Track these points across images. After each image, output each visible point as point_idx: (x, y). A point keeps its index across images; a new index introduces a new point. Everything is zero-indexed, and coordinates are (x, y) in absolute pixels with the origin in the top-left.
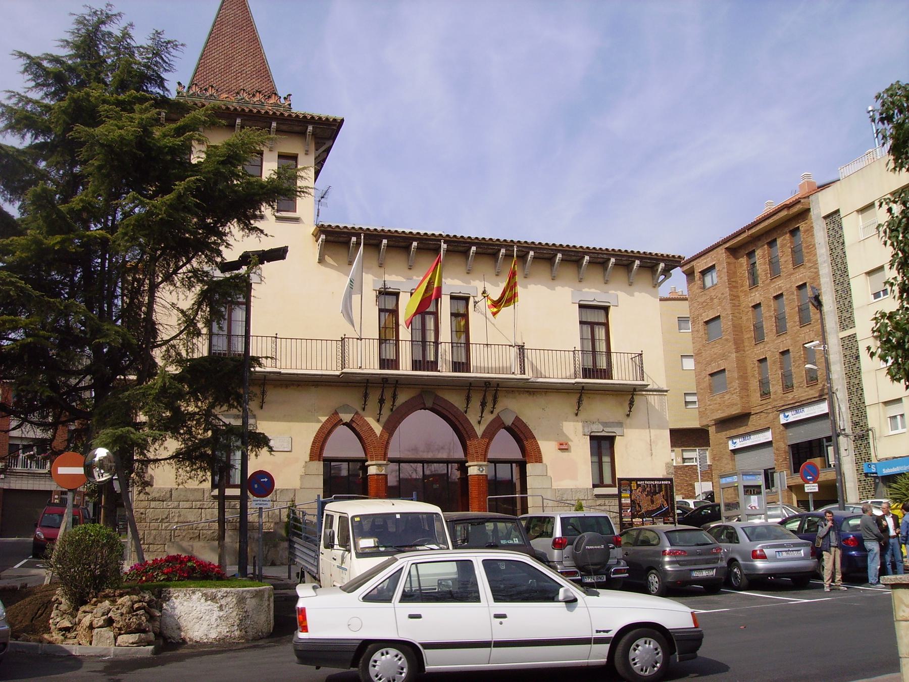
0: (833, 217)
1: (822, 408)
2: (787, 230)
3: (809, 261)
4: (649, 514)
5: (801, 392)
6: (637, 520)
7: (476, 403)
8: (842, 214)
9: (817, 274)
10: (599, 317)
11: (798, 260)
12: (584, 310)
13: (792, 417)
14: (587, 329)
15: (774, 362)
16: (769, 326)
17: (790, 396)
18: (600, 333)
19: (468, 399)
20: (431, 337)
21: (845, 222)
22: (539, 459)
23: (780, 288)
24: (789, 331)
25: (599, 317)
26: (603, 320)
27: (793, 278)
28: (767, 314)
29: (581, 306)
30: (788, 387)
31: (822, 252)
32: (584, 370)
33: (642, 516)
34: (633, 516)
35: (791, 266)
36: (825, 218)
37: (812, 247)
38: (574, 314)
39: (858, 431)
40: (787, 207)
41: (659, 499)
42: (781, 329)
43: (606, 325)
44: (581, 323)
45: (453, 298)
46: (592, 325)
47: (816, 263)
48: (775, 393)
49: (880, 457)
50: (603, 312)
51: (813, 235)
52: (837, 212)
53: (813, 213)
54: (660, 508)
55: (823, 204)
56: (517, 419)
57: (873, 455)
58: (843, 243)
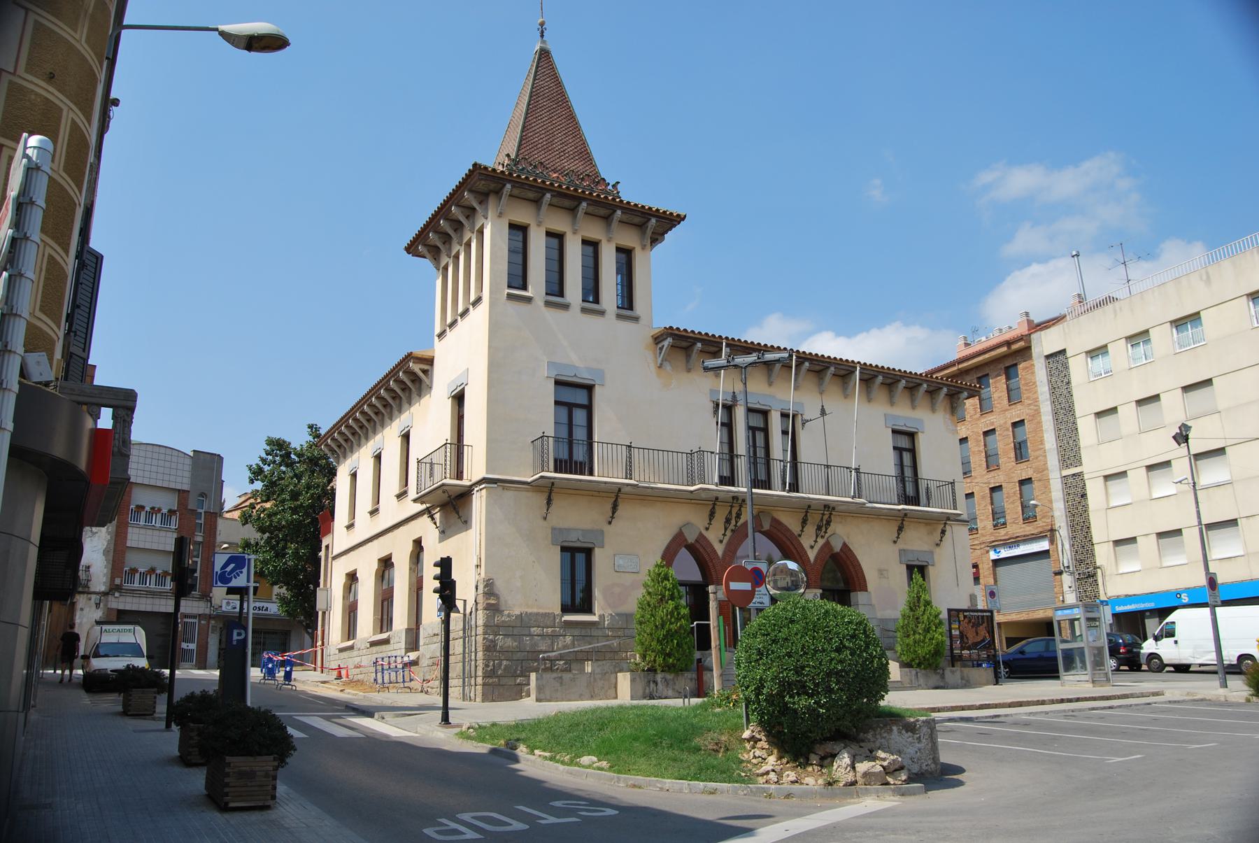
0: (1058, 357)
1: (1044, 545)
2: (1002, 366)
3: (1028, 398)
4: (975, 646)
5: (1016, 527)
6: (966, 652)
7: (810, 530)
8: (1069, 354)
9: (1038, 412)
10: (580, 397)
11: (1013, 397)
12: (560, 387)
13: (1005, 553)
14: (564, 411)
15: (983, 497)
16: (978, 461)
17: (1002, 532)
18: (580, 416)
19: (804, 522)
20: (580, 434)
21: (1072, 363)
22: (864, 588)
23: (992, 424)
24: (1002, 467)
25: (580, 397)
26: (585, 402)
27: (1008, 414)
28: (976, 449)
29: (894, 431)
30: (998, 518)
31: (1043, 390)
32: (721, 477)
33: (969, 649)
34: (962, 648)
35: (1006, 401)
36: (1048, 357)
37: (1033, 385)
38: (888, 441)
39: (1083, 569)
40: (1008, 343)
41: (983, 631)
42: (991, 462)
43: (589, 408)
44: (557, 403)
45: (750, 410)
46: (570, 407)
47: (1036, 400)
48: (984, 528)
49: (1109, 594)
50: (584, 393)
51: (1033, 373)
52: (1063, 352)
53: (1035, 351)
54: (983, 640)
55: (1045, 343)
56: (845, 545)
57: (1102, 592)
58: (1068, 383)
